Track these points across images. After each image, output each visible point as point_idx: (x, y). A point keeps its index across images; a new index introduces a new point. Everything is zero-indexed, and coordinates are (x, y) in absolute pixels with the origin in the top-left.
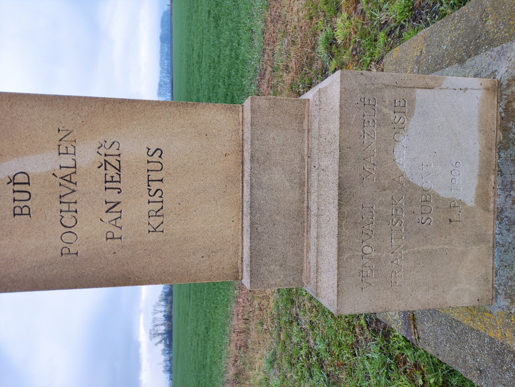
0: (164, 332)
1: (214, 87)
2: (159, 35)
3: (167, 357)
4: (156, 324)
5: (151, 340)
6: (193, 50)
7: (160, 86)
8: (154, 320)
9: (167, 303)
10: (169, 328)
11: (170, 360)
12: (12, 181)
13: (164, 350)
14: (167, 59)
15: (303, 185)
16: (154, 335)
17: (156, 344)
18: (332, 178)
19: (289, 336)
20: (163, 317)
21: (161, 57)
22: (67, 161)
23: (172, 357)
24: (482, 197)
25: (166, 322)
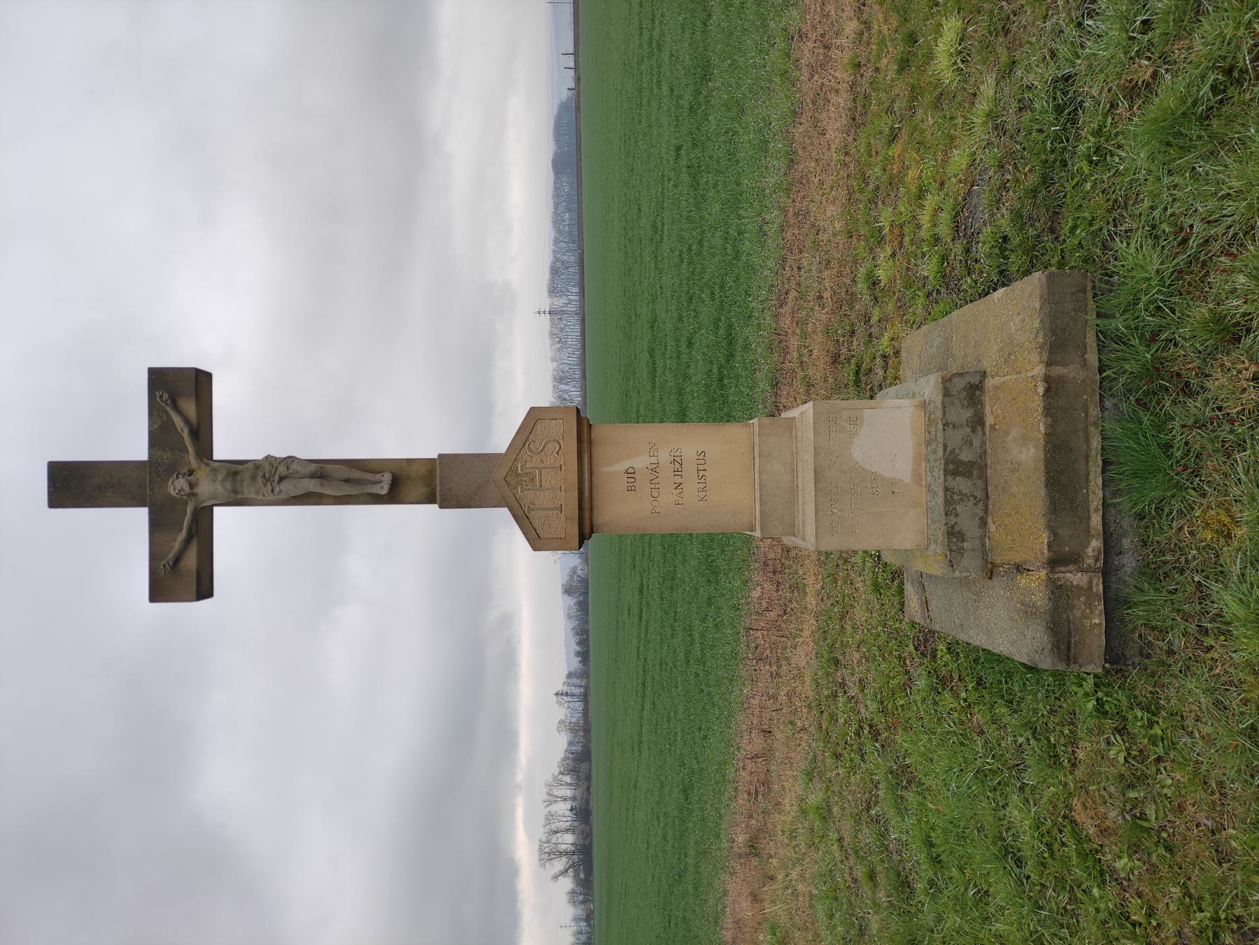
0: (572, 848)
1: (691, 299)
2: (551, 156)
3: (579, 911)
4: (554, 827)
5: (543, 865)
6: (640, 210)
7: (554, 271)
8: (550, 817)
9: (578, 778)
10: (584, 839)
11: (588, 918)
12: (627, 472)
13: (573, 892)
14: (569, 210)
15: (793, 471)
16: (549, 854)
17: (555, 877)
18: (810, 466)
19: (834, 718)
20: (568, 813)
21: (556, 206)
22: (654, 460)
23: (592, 912)
24: (917, 477)
25: (576, 824)
